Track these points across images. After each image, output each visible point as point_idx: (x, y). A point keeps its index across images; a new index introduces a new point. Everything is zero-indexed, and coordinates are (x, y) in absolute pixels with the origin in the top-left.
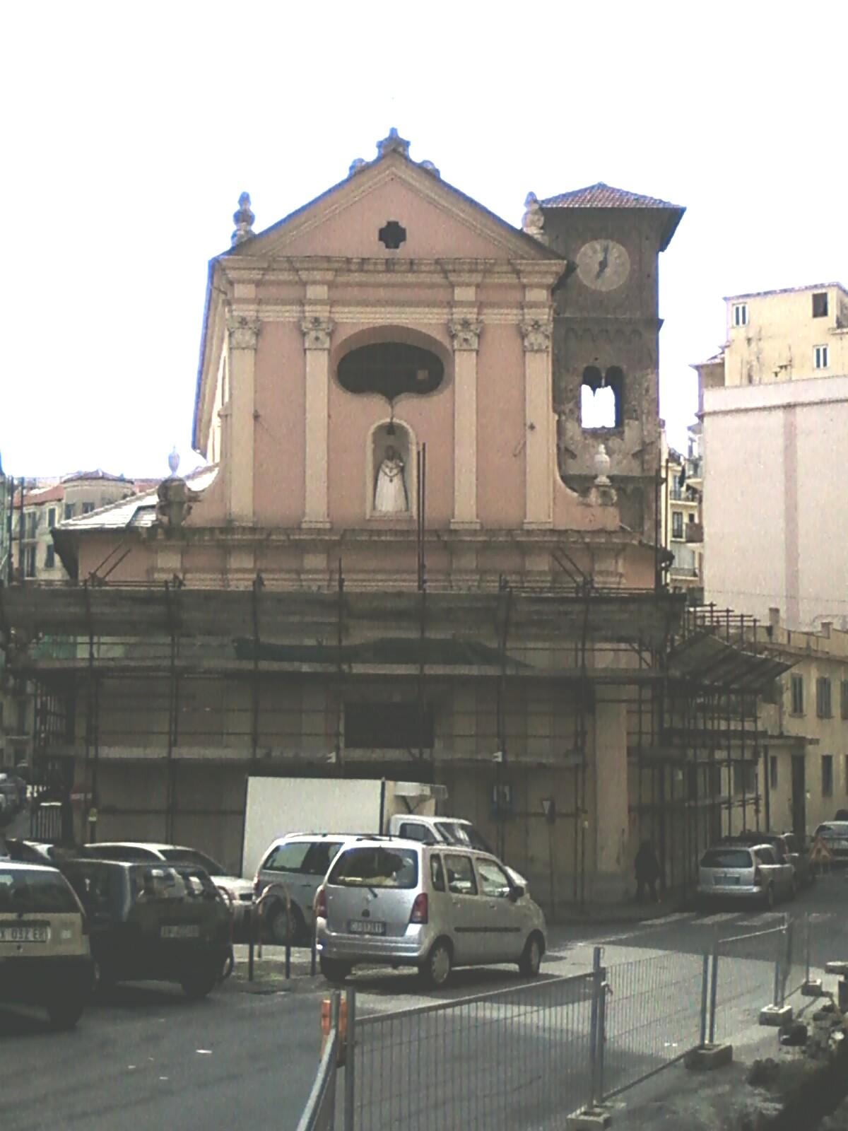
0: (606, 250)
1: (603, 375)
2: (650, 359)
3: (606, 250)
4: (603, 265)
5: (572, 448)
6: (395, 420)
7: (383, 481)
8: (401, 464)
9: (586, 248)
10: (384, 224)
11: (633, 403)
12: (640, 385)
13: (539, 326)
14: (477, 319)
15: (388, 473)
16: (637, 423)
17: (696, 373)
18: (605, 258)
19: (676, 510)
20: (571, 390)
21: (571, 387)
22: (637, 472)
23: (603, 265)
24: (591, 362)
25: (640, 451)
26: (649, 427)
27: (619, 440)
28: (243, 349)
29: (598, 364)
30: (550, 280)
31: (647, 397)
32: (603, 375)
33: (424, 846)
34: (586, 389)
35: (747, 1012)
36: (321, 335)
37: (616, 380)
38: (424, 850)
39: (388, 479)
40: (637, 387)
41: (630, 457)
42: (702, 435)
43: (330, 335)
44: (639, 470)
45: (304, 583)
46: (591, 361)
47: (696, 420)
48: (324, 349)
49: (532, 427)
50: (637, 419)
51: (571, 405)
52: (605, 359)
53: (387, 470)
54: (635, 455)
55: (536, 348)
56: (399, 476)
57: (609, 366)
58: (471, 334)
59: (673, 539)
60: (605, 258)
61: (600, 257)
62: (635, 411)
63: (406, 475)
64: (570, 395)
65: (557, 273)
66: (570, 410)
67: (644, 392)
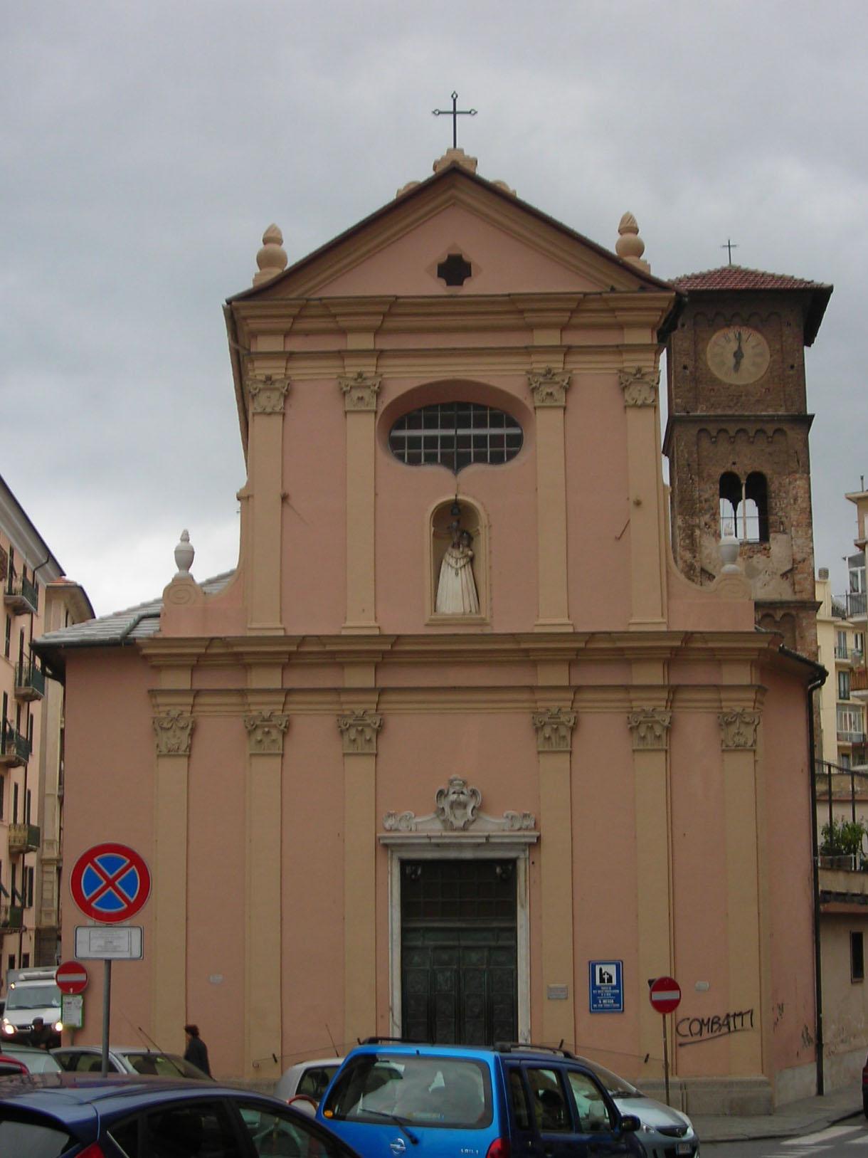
0: (739, 339)
1: (744, 482)
2: (800, 462)
3: (739, 339)
4: (738, 355)
5: (709, 568)
6: (460, 497)
7: (447, 575)
8: (470, 553)
9: (717, 337)
10: (444, 259)
11: (780, 514)
12: (787, 492)
13: (643, 375)
14: (563, 369)
15: (454, 565)
16: (785, 536)
17: (854, 507)
18: (740, 348)
19: (840, 670)
20: (706, 501)
21: (706, 496)
22: (787, 595)
23: (738, 355)
24: (728, 467)
25: (791, 570)
26: (800, 542)
27: (764, 557)
28: (270, 414)
29: (735, 469)
30: (656, 317)
31: (796, 507)
32: (744, 482)
33: (497, 1054)
34: (725, 505)
35: (731, 397)
36: (366, 394)
37: (758, 488)
38: (496, 1059)
39: (454, 571)
40: (784, 495)
41: (778, 577)
42: (864, 568)
43: (378, 394)
44: (790, 590)
45: (345, 707)
46: (729, 465)
47: (857, 551)
48: (369, 411)
49: (638, 503)
50: (784, 532)
51: (707, 517)
52: (745, 462)
53: (452, 561)
54: (784, 575)
55: (639, 402)
56: (468, 568)
57: (749, 472)
58: (557, 387)
59: (841, 701)
60: (740, 348)
61: (734, 346)
62: (782, 523)
63: (476, 567)
64: (706, 506)
65: (663, 310)
66: (706, 524)
67: (792, 501)
